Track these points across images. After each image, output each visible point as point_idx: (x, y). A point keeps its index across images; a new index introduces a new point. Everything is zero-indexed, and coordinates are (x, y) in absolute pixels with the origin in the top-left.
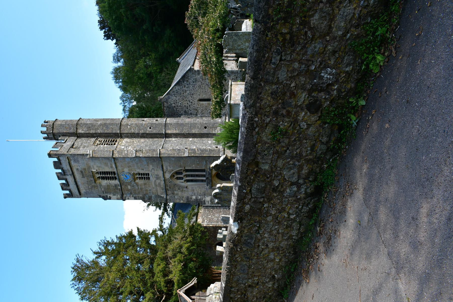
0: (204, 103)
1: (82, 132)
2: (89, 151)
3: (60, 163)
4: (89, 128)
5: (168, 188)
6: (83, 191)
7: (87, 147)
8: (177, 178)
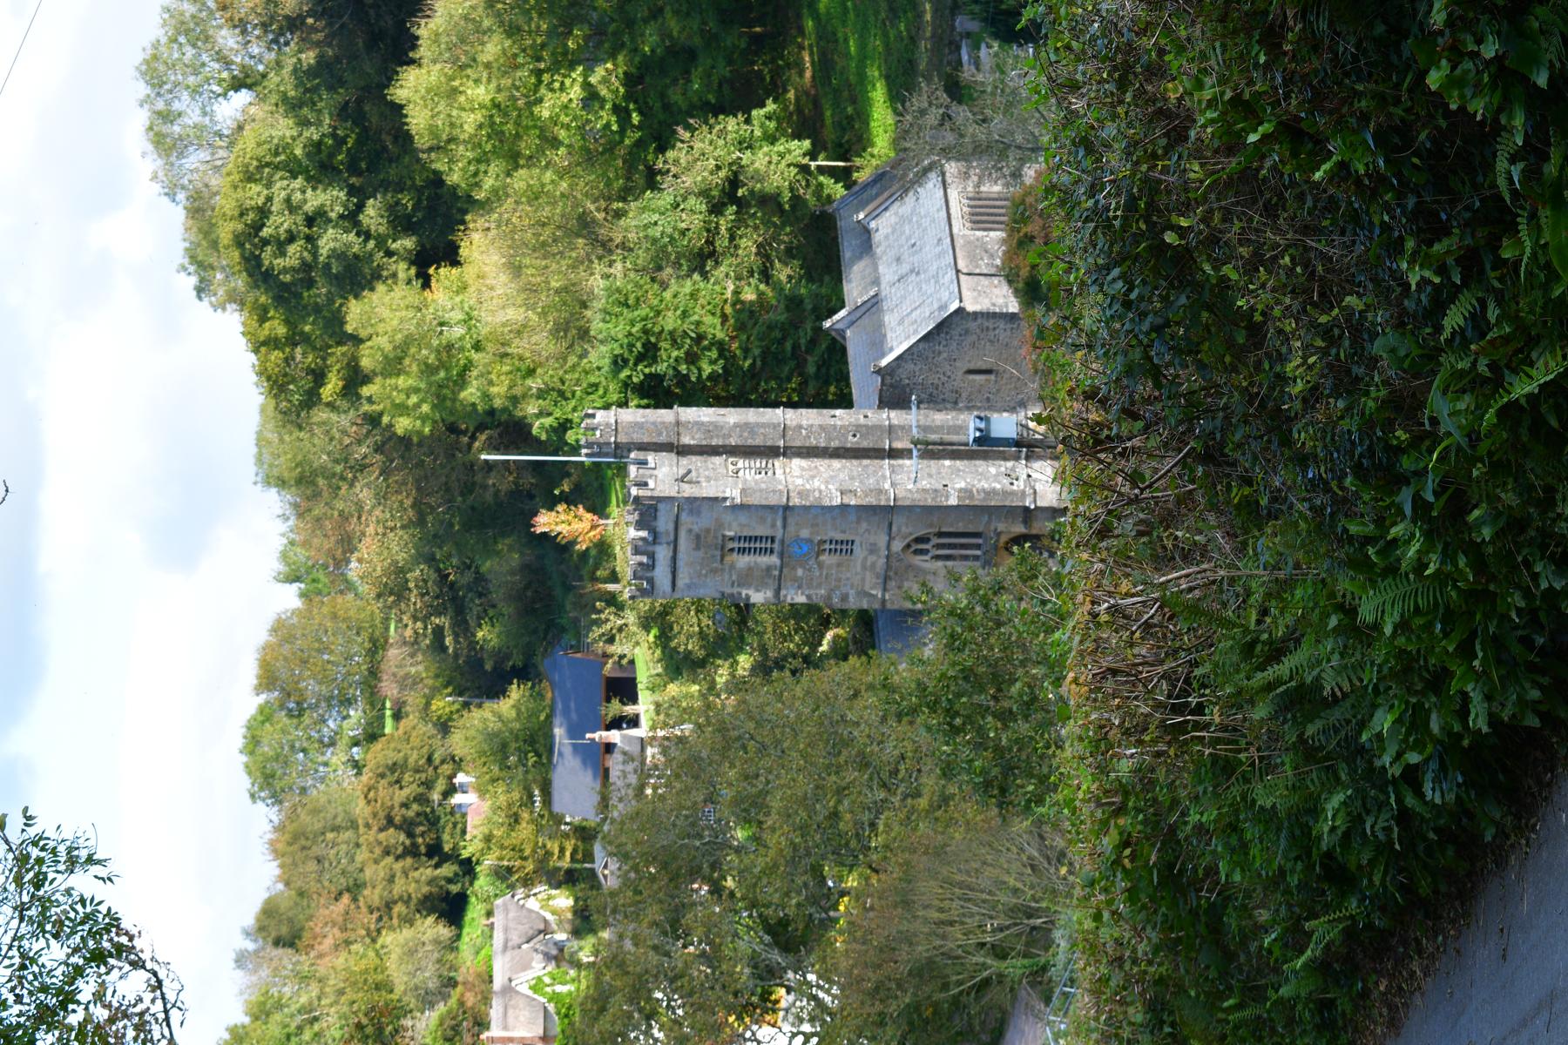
0: (978, 377)
2: (733, 493)
8: (916, 552)
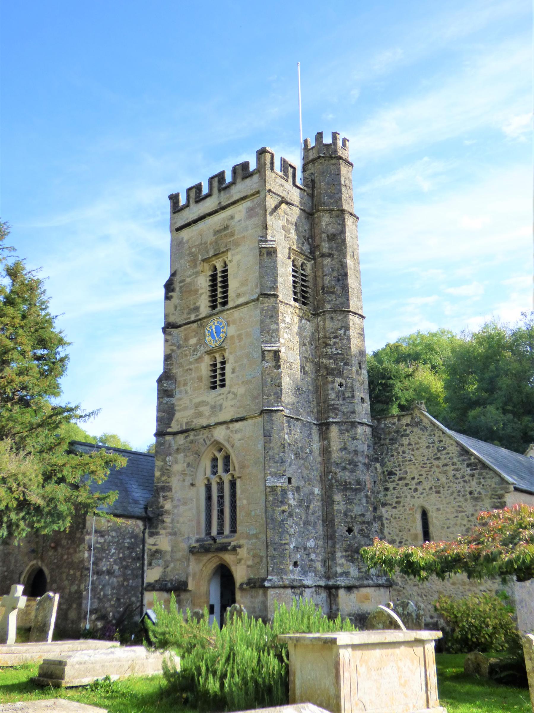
1: (323, 224)
3: (246, 178)
4: (332, 238)
5: (191, 437)
6: (185, 234)
7: (283, 233)
8: (215, 459)
